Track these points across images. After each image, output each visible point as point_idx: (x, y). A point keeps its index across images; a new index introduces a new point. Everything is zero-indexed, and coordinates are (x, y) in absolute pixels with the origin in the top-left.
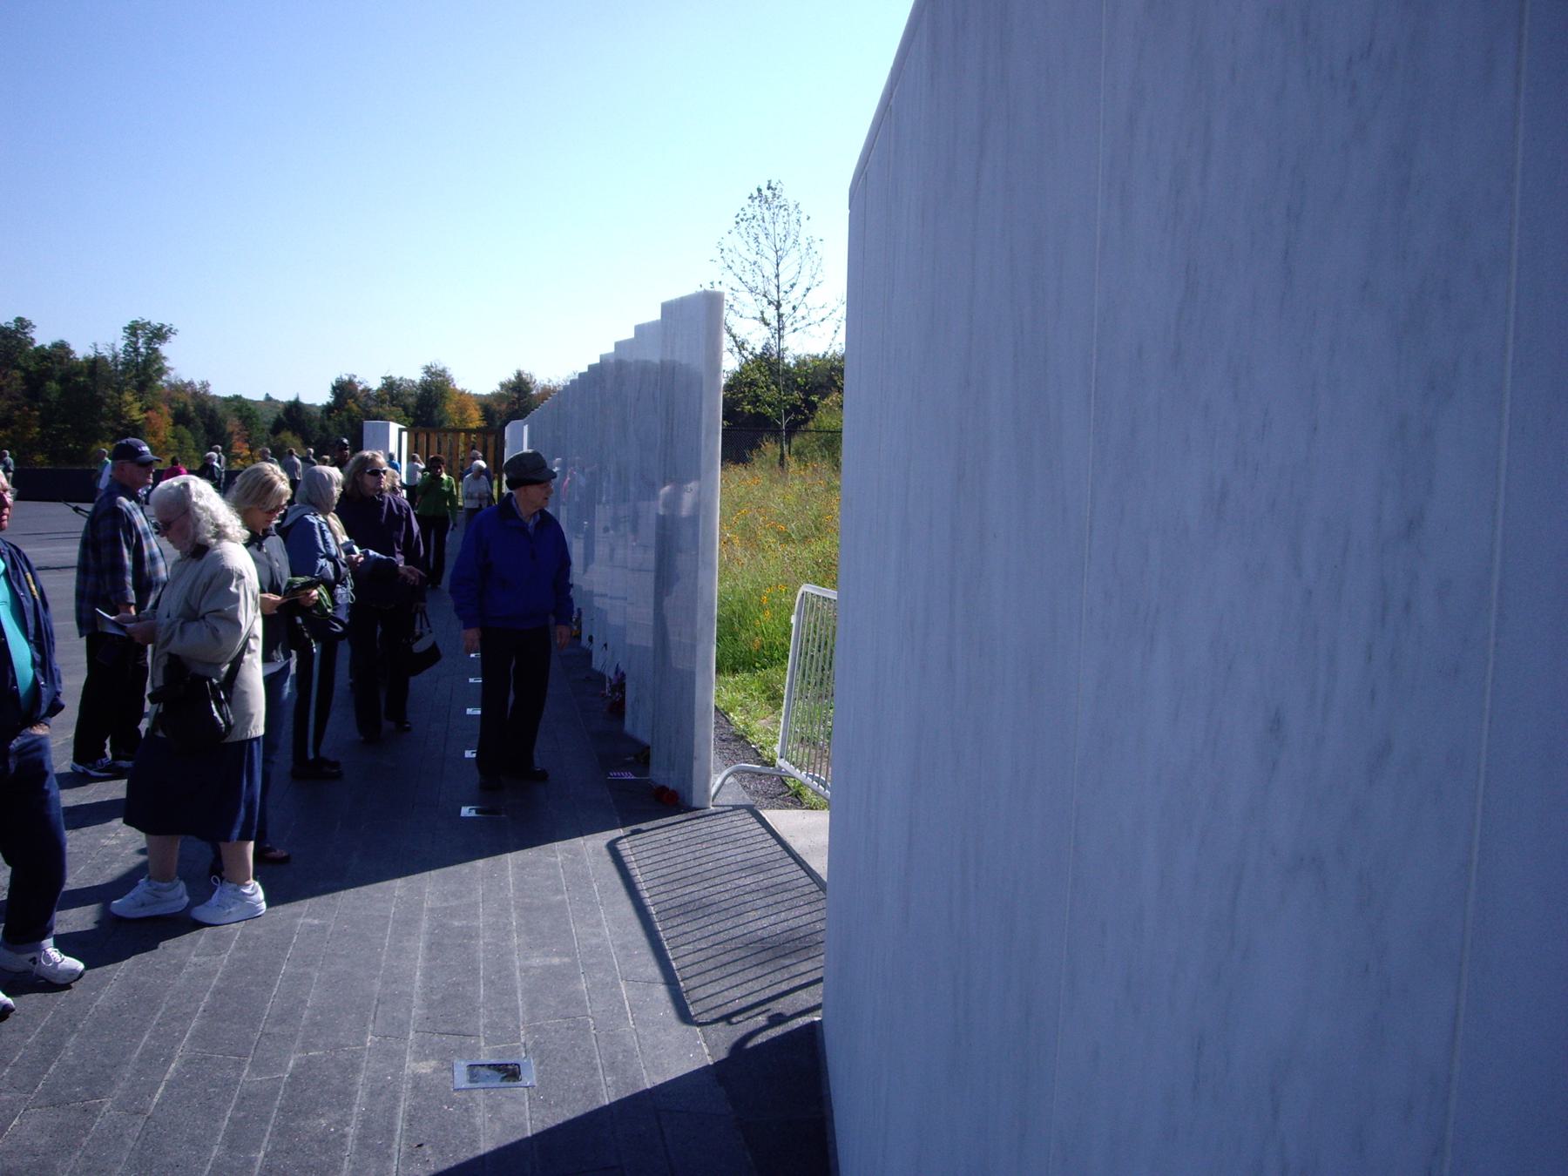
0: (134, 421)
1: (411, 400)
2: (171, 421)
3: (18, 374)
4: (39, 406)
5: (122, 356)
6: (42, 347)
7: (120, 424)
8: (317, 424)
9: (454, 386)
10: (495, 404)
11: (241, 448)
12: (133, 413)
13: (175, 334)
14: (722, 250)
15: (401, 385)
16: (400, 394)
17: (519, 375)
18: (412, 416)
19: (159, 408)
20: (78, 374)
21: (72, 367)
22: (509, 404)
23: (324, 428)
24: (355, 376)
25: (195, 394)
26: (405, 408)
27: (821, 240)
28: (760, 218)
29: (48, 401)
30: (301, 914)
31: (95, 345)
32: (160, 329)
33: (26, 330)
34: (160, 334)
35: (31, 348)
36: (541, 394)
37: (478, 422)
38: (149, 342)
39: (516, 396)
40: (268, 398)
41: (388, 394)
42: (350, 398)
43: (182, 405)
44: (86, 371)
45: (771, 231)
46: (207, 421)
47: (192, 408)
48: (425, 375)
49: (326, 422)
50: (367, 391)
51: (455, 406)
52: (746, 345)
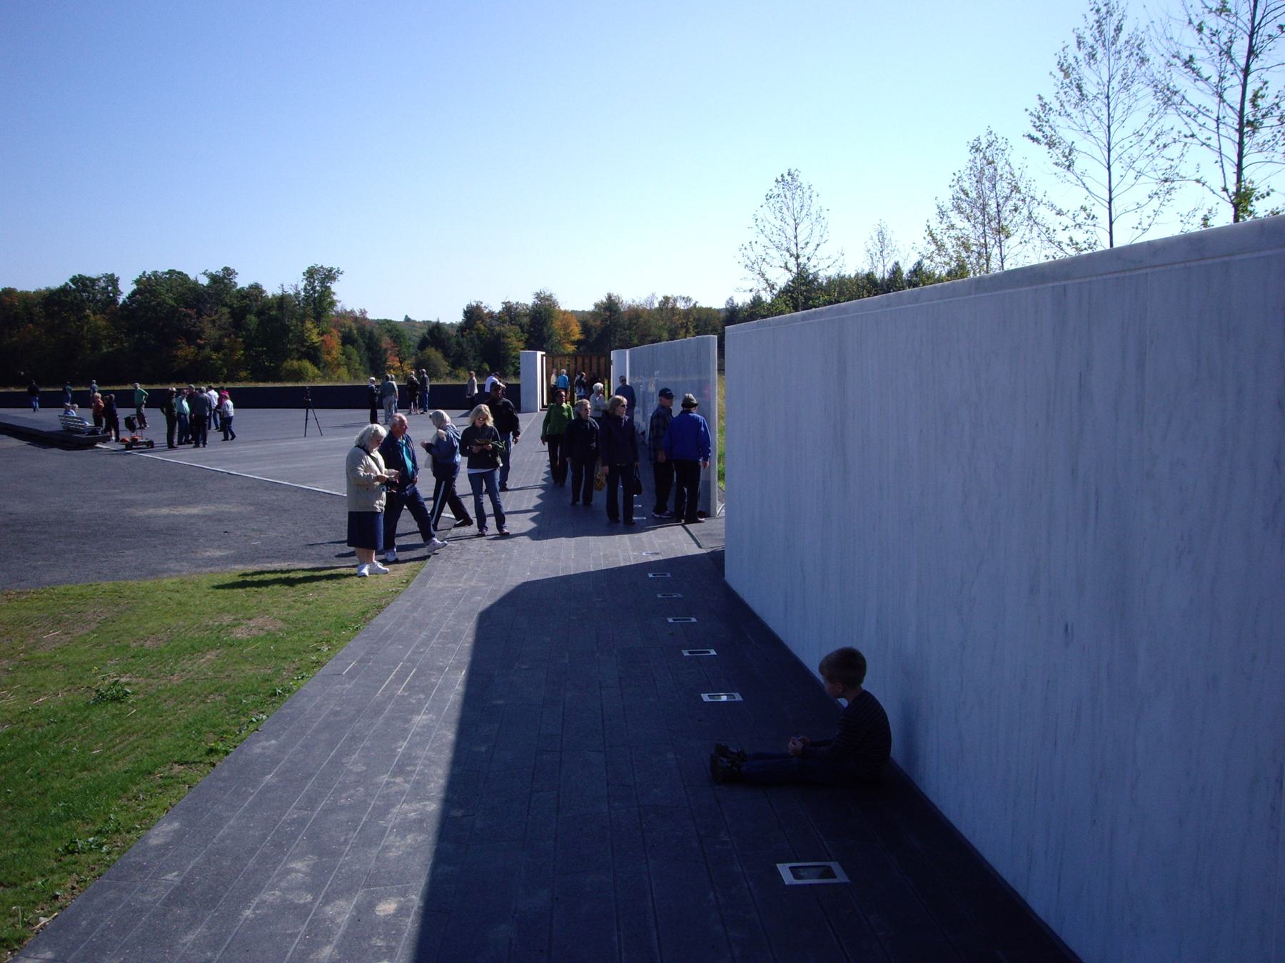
0: (314, 343)
1: (526, 320)
2: (340, 341)
3: (226, 310)
4: (242, 334)
5: (303, 293)
6: (243, 288)
7: (303, 346)
8: (453, 340)
9: (559, 307)
10: (591, 321)
11: (393, 361)
12: (313, 337)
13: (341, 273)
14: (757, 220)
15: (517, 308)
16: (518, 315)
17: (610, 297)
18: (527, 333)
19: (331, 332)
20: (270, 308)
21: (265, 303)
22: (602, 321)
23: (459, 344)
24: (482, 303)
25: (356, 319)
26: (521, 326)
27: (828, 210)
28: (783, 195)
29: (249, 330)
30: (414, 771)
31: (282, 286)
32: (331, 271)
33: (231, 277)
34: (330, 275)
35: (234, 290)
36: (627, 311)
37: (578, 336)
38: (322, 282)
39: (608, 314)
40: (407, 319)
41: (507, 315)
42: (478, 320)
43: (347, 329)
44: (275, 306)
45: (791, 205)
46: (367, 341)
47: (355, 332)
48: (536, 300)
49: (461, 339)
50: (491, 314)
51: (560, 324)
52: (775, 286)
